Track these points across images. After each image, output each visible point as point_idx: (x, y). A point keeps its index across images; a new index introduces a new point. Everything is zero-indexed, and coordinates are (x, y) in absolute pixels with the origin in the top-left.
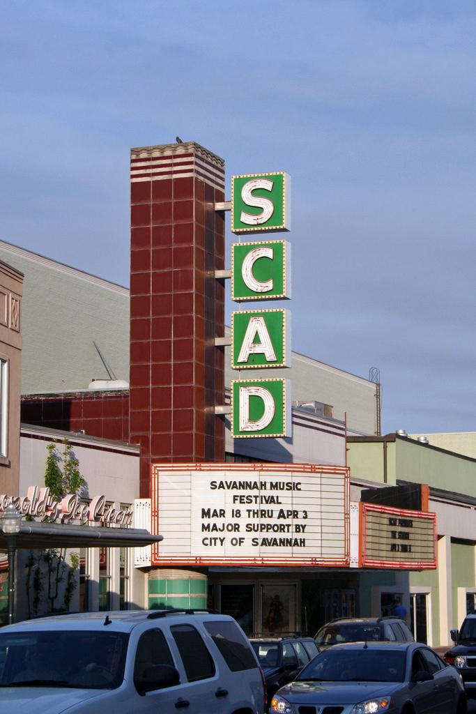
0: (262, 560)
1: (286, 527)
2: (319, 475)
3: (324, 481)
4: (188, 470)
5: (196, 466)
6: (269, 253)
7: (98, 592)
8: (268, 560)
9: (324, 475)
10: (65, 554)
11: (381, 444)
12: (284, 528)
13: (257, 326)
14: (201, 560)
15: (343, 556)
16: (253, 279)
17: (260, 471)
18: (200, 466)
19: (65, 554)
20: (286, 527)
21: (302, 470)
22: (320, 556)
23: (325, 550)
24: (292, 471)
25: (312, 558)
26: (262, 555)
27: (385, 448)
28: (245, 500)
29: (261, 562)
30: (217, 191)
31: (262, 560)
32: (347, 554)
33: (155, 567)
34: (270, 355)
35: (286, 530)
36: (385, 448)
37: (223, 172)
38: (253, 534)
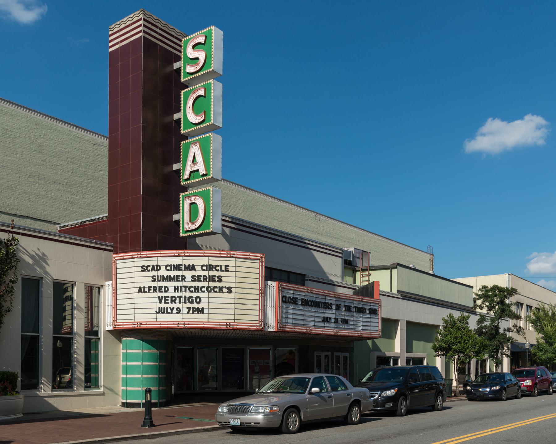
0: (184, 324)
1: (178, 299)
2: (234, 259)
3: (238, 264)
4: (133, 258)
5: (138, 254)
6: (202, 92)
7: (201, 316)
8: (189, 324)
9: (237, 259)
10: (263, 292)
11: (389, 271)
12: (176, 299)
13: (195, 150)
14: (142, 324)
15: (258, 322)
16: (193, 115)
17: (183, 256)
18: (230, 254)
19: (263, 292)
20: (178, 299)
21: (202, 255)
22: (233, 321)
23: (237, 317)
24: (209, 256)
25: (227, 323)
26: (183, 320)
27: (391, 272)
28: (216, 279)
29: (183, 326)
30: (176, 54)
31: (184, 324)
32: (264, 320)
33: (117, 310)
34: (202, 171)
35: (177, 301)
36: (391, 272)
37: (180, 46)
38: (200, 306)
